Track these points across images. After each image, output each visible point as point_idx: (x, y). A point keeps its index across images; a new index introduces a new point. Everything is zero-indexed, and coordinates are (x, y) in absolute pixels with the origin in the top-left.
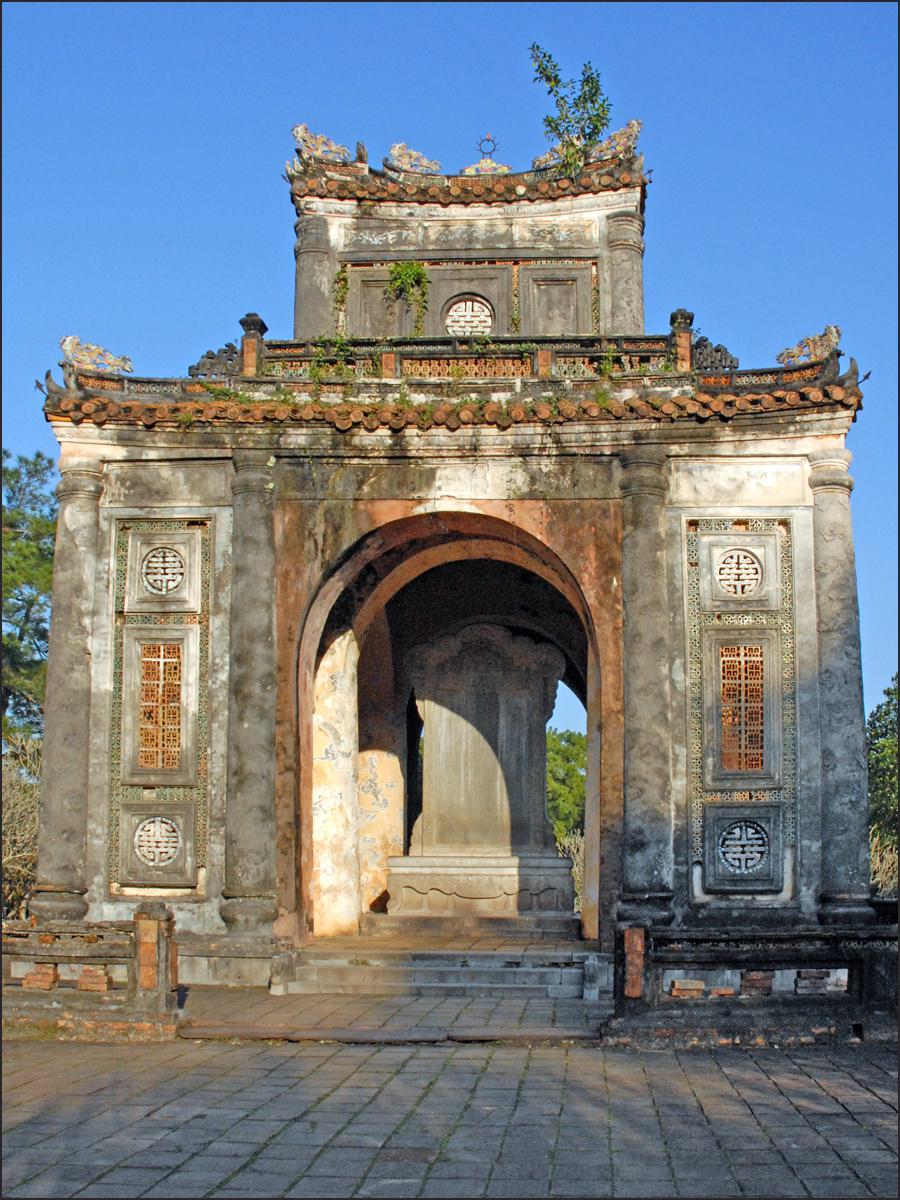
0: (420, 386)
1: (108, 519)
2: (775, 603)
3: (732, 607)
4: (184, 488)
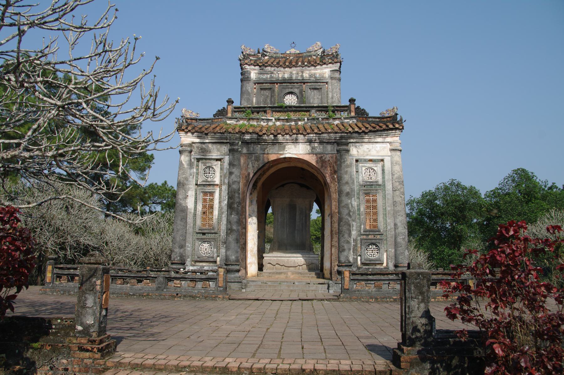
0: (278, 120)
1: (194, 158)
2: (380, 182)
3: (368, 183)
4: (215, 150)
